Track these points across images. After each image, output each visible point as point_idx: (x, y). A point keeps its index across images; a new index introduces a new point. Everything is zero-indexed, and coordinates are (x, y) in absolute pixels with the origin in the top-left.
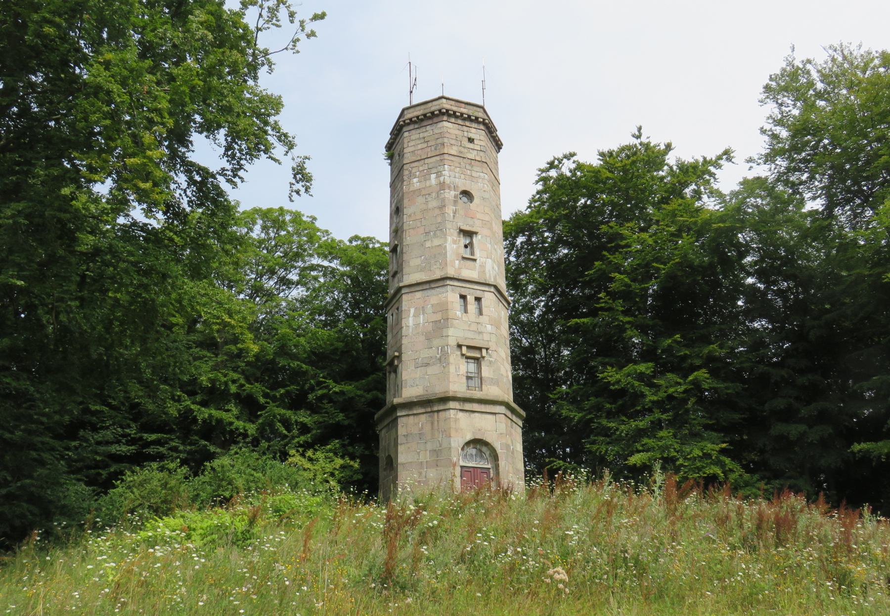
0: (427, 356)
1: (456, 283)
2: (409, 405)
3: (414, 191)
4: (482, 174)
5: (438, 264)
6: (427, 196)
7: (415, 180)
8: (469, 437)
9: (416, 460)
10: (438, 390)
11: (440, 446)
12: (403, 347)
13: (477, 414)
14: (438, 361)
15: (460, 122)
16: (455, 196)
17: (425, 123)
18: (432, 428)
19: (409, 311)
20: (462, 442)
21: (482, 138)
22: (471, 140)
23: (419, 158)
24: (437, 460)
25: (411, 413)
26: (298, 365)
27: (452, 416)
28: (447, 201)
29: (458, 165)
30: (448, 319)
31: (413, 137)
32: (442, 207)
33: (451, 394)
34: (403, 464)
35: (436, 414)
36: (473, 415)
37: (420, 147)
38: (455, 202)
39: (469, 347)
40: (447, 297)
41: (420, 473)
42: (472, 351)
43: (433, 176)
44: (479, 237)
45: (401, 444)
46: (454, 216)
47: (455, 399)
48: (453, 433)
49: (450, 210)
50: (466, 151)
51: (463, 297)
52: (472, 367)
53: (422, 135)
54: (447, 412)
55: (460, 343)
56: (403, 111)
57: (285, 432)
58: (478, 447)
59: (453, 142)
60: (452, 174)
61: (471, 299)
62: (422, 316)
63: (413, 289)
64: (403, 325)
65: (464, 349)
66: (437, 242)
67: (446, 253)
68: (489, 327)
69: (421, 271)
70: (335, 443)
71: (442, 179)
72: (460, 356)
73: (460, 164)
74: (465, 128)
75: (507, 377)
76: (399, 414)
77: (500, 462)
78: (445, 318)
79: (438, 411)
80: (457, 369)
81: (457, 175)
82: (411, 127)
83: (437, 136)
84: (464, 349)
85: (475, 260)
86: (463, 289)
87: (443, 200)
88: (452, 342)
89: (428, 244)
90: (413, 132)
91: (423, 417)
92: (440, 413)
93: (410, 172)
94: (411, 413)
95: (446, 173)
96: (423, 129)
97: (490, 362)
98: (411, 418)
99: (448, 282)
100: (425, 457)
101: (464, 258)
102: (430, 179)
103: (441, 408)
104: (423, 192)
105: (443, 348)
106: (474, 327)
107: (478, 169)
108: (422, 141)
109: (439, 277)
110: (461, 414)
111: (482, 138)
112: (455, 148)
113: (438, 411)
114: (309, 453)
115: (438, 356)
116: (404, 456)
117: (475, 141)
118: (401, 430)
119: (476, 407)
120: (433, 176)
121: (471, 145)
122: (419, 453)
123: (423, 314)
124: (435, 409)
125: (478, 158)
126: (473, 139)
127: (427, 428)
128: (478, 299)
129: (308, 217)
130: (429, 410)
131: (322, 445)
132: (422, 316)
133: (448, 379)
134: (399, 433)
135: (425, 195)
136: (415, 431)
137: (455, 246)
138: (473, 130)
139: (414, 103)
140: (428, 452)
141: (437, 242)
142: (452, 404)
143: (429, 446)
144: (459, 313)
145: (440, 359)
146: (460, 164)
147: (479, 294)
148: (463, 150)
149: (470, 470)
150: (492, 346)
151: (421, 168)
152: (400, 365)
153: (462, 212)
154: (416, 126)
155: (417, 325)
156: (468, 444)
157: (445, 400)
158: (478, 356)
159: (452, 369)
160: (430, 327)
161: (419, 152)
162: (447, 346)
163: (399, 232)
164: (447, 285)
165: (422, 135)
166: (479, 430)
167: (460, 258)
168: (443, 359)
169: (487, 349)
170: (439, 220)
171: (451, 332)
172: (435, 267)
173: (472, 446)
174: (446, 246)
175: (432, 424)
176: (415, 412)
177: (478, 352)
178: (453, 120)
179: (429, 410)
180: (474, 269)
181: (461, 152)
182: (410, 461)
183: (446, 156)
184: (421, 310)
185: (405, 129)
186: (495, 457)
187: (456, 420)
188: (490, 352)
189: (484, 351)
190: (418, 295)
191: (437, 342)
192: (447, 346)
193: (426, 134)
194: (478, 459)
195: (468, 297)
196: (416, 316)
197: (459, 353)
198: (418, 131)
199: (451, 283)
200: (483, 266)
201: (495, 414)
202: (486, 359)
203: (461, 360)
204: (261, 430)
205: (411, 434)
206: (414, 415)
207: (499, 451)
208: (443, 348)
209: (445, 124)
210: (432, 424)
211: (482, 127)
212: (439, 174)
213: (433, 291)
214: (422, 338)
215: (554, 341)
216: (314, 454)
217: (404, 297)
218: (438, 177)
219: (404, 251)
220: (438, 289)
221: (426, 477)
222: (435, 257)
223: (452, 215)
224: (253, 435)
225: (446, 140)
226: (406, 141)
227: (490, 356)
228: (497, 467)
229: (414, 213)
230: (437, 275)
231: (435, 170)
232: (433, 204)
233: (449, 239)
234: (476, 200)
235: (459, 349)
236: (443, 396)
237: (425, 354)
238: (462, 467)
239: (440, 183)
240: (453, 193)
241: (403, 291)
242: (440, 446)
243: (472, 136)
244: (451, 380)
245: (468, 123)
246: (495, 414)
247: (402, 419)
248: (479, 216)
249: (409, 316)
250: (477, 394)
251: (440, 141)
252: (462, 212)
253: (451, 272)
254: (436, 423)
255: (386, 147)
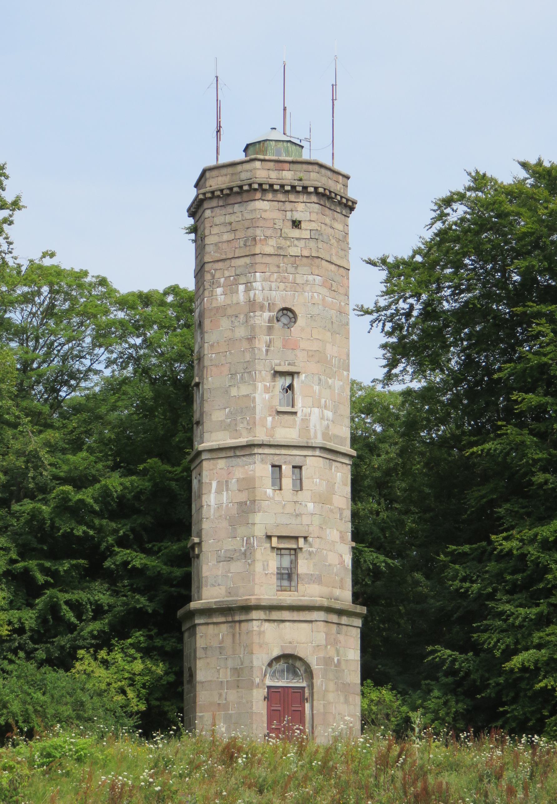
0: (230, 548)
1: (267, 451)
2: (208, 612)
3: (217, 309)
4: (310, 278)
5: (245, 423)
6: (233, 319)
7: (219, 291)
8: (276, 652)
9: (215, 679)
10: (241, 598)
11: (242, 664)
12: (204, 533)
13: (287, 624)
14: (243, 556)
15: (281, 197)
16: (270, 321)
17: (232, 200)
18: (234, 642)
19: (211, 484)
20: (266, 659)
21: (314, 217)
22: (296, 224)
23: (224, 257)
24: (238, 681)
25: (210, 621)
26: (84, 532)
27: (255, 628)
28: (257, 330)
29: (276, 269)
30: (255, 501)
31: (217, 220)
32: (251, 339)
33: (253, 603)
34: (202, 683)
35: (237, 625)
36: (282, 625)
37: (226, 237)
38: (270, 329)
39: (279, 537)
40: (254, 471)
41: (220, 695)
42: (284, 541)
43: (241, 288)
44: (303, 377)
45: (200, 658)
46: (267, 351)
47: (258, 608)
48: (256, 649)
49: (261, 343)
50: (288, 243)
51: (277, 467)
52: (286, 562)
53: (228, 219)
54: (250, 624)
55: (269, 534)
56: (204, 172)
57: (73, 620)
58: (290, 662)
59: (269, 233)
60: (266, 285)
61: (286, 469)
62: (225, 493)
63: (214, 455)
64: (204, 503)
65: (274, 540)
66: (244, 390)
67: (255, 407)
68: (311, 506)
69: (225, 429)
70: (139, 636)
71: (252, 293)
72: (269, 549)
73: (278, 267)
74: (288, 206)
75: (342, 562)
76: (197, 621)
77: (315, 681)
78: (252, 499)
79: (240, 622)
80: (265, 567)
81: (274, 285)
82: (214, 203)
83: (247, 224)
84: (274, 540)
85: (295, 413)
86: (276, 458)
87: (253, 328)
88: (259, 531)
89: (234, 392)
90: (217, 211)
91: (224, 627)
92: (243, 624)
93: (213, 276)
94: (210, 621)
95: (257, 285)
96: (229, 209)
97: (310, 553)
98: (211, 627)
99: (256, 450)
100: (225, 676)
101: (279, 413)
102: (237, 292)
103: (243, 617)
104: (229, 312)
105: (248, 539)
106: (289, 509)
107: (305, 270)
108: (229, 228)
109: (245, 444)
110: (267, 625)
111: (314, 217)
112: (272, 242)
113: (240, 622)
114: (103, 654)
115: (243, 549)
116: (200, 676)
117: (303, 225)
118: (200, 642)
119: (286, 615)
120: (241, 288)
121: (296, 233)
122: (218, 671)
123: (227, 490)
124: (237, 618)
125: (306, 253)
126: (300, 222)
127: (228, 641)
128: (298, 467)
129: (93, 277)
130: (230, 619)
131: (120, 639)
132: (225, 493)
133: (254, 580)
134: (198, 645)
135: (231, 316)
136: (215, 644)
137: (267, 396)
138: (301, 207)
139: (222, 161)
140: (229, 670)
141: (244, 390)
142: (255, 614)
143: (230, 663)
144: (269, 491)
145: (245, 554)
146: (278, 267)
147: (297, 461)
148: (283, 242)
149: (280, 690)
150: (314, 531)
151: (227, 274)
152: (201, 555)
153: (278, 343)
154: (221, 203)
155: (219, 507)
156: (277, 659)
157: (246, 609)
158: (294, 546)
159: (258, 567)
160: (234, 510)
161: (225, 246)
162: (253, 537)
163: (201, 360)
164: (255, 454)
165: (228, 219)
166: (290, 643)
167: (274, 413)
168: (248, 553)
169: (305, 538)
170: (248, 357)
171: (258, 518)
172: (242, 425)
173: (282, 661)
174: (254, 398)
175: (234, 635)
176: (215, 620)
177: (293, 541)
178: (270, 196)
179: (230, 619)
180: (292, 426)
181: (280, 248)
182: (209, 678)
183: (258, 259)
184: (224, 485)
185: (206, 205)
186: (309, 673)
187: (260, 633)
188: (310, 539)
189: (301, 541)
190: (221, 463)
191: (242, 531)
192: (253, 537)
193: (232, 218)
194: (291, 676)
195: (284, 467)
196: (219, 492)
197: (268, 545)
198: (223, 211)
199: (260, 451)
200: (306, 421)
201: (311, 622)
202: (304, 550)
203: (271, 554)
204: (42, 620)
205: (211, 647)
206: (214, 623)
207: (315, 667)
208: (248, 539)
209: (260, 205)
210: (234, 635)
211: (314, 198)
212: (249, 286)
213: (238, 460)
214: (225, 524)
215: (496, 425)
216: (109, 655)
217: (205, 464)
218: (247, 290)
219: (205, 398)
220: (244, 459)
221: (226, 699)
222: (242, 412)
223: (264, 350)
224: (31, 630)
225: (258, 232)
226: (207, 225)
227: (311, 546)
228: (311, 686)
229: (218, 343)
230: (242, 441)
231: (243, 280)
232: (241, 332)
233: (260, 385)
234: (301, 321)
235: (268, 541)
236: (244, 604)
237: (230, 545)
238: (269, 687)
239: (250, 301)
240: (267, 315)
241: (204, 456)
242: (242, 664)
243: (297, 216)
244: (257, 581)
245: (292, 197)
246: (311, 622)
247: (200, 627)
248: (303, 344)
249: (210, 491)
250: (288, 598)
251: (250, 232)
252: (278, 343)
253: (261, 436)
254: (237, 635)
255: (188, 211)
